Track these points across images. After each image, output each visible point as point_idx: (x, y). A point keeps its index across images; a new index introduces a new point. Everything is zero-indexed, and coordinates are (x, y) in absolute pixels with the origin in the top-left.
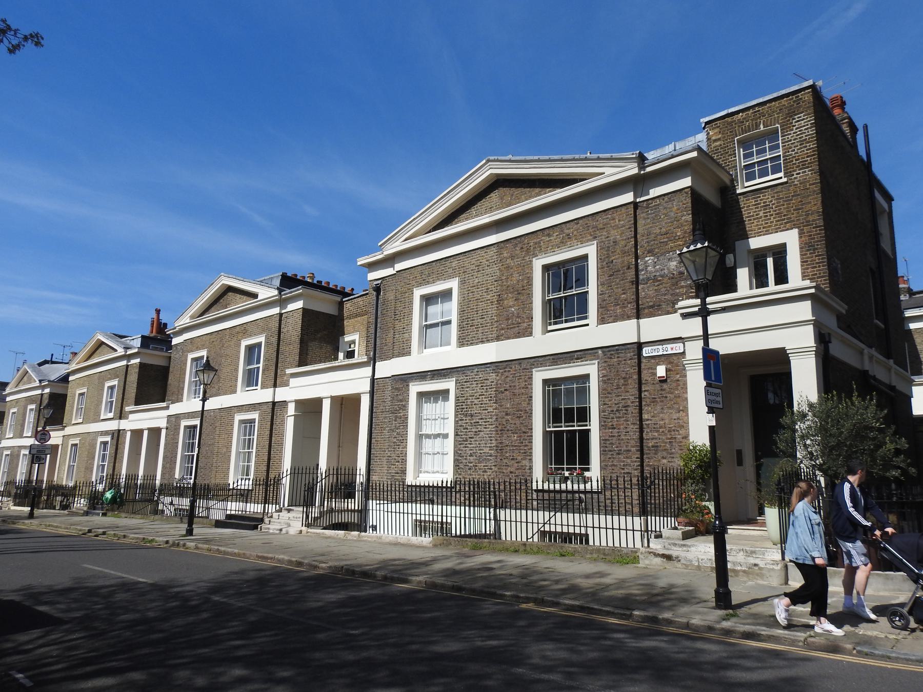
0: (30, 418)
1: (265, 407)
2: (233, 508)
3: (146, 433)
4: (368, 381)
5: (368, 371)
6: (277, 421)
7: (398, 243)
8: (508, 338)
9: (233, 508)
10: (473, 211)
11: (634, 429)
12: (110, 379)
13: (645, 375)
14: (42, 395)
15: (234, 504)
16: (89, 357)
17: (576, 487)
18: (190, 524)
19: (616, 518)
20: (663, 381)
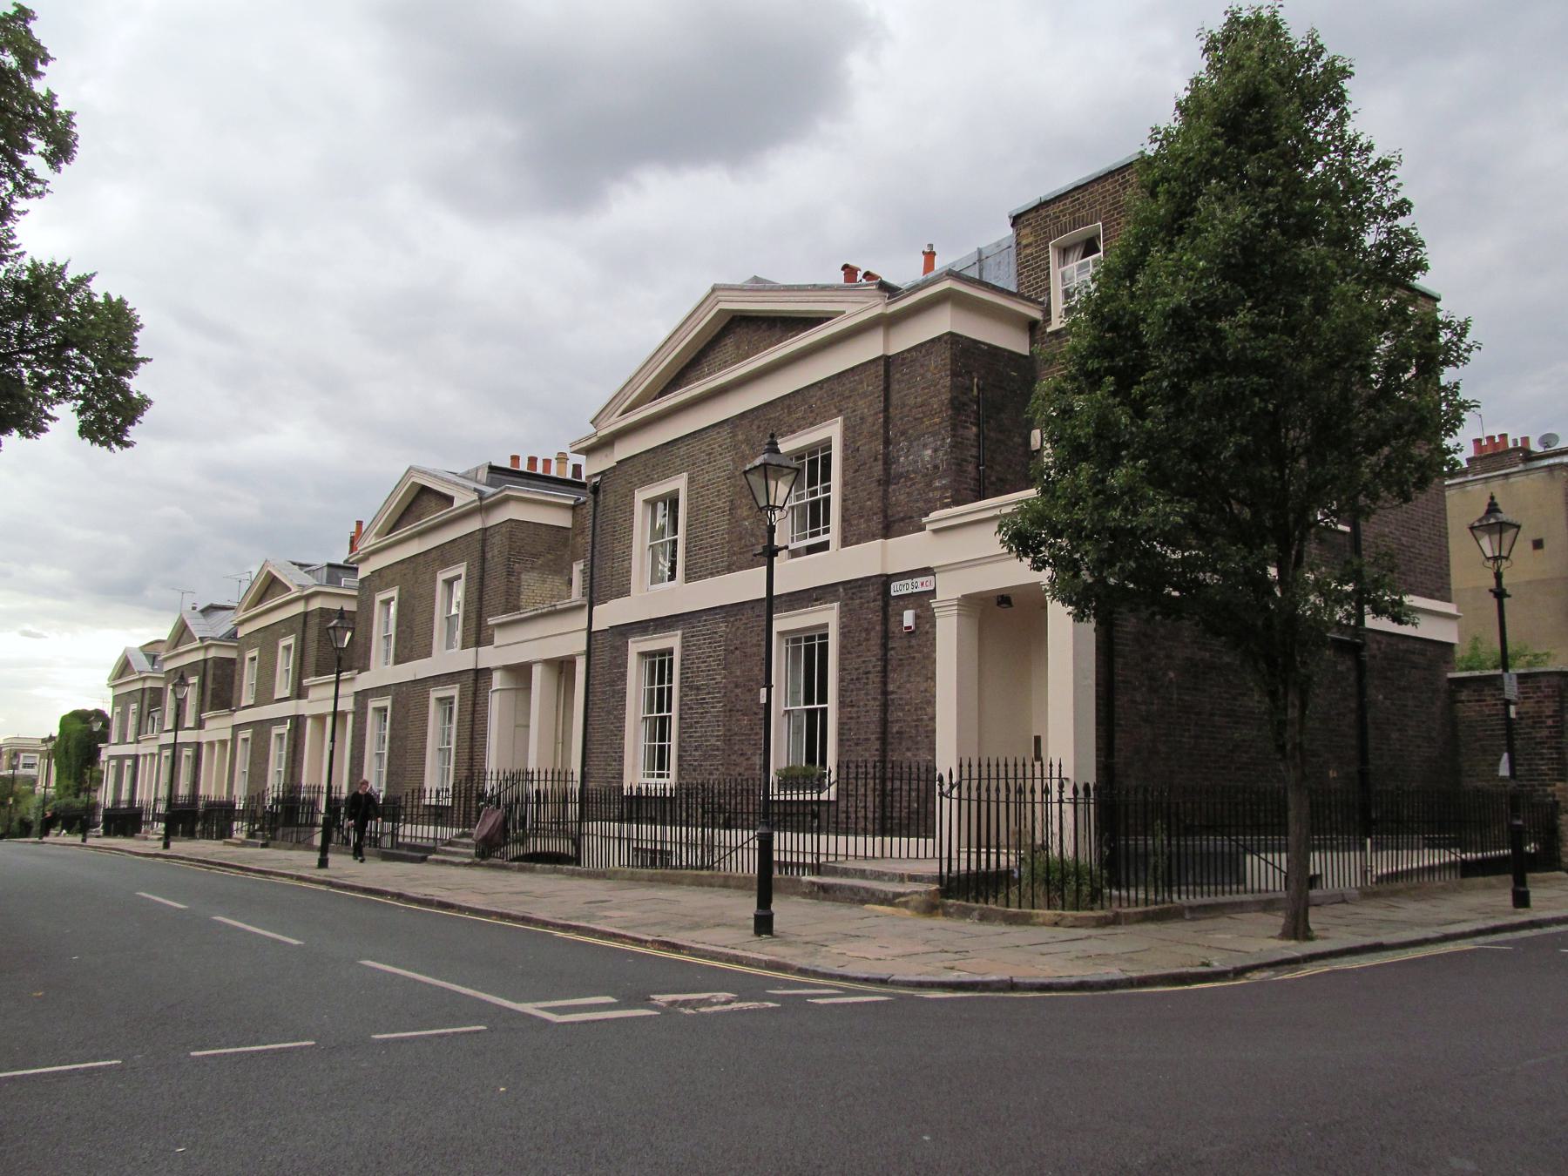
0: (285, 664)
1: (464, 678)
2: (408, 833)
3: (537, 671)
4: (584, 635)
5: (581, 620)
6: (480, 699)
7: (614, 418)
8: (741, 569)
9: (408, 833)
10: (719, 355)
11: (874, 705)
12: (285, 635)
13: (893, 627)
14: (205, 661)
15: (408, 826)
16: (176, 646)
17: (808, 797)
18: (764, 901)
19: (842, 839)
20: (911, 633)
